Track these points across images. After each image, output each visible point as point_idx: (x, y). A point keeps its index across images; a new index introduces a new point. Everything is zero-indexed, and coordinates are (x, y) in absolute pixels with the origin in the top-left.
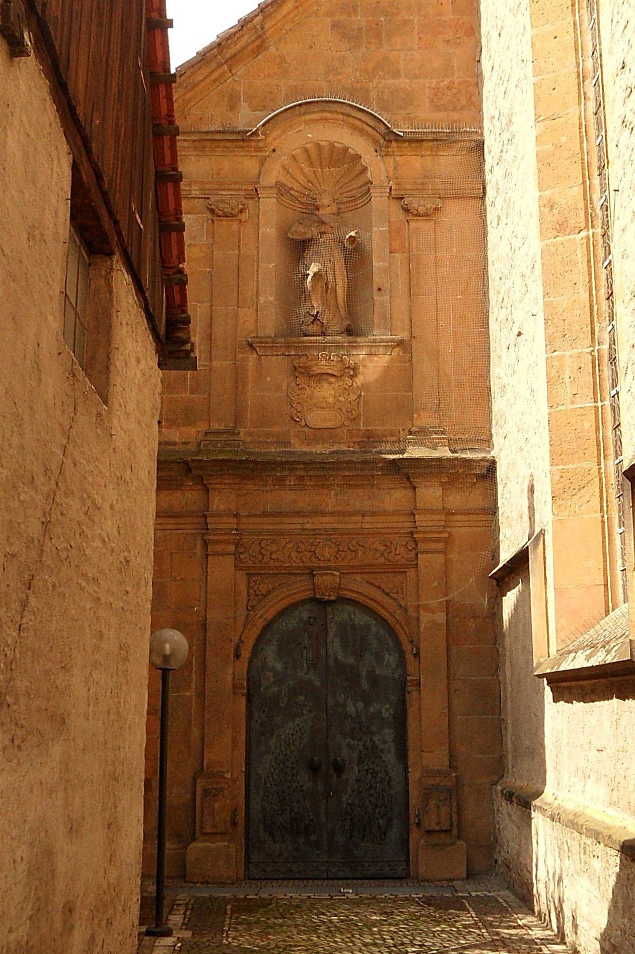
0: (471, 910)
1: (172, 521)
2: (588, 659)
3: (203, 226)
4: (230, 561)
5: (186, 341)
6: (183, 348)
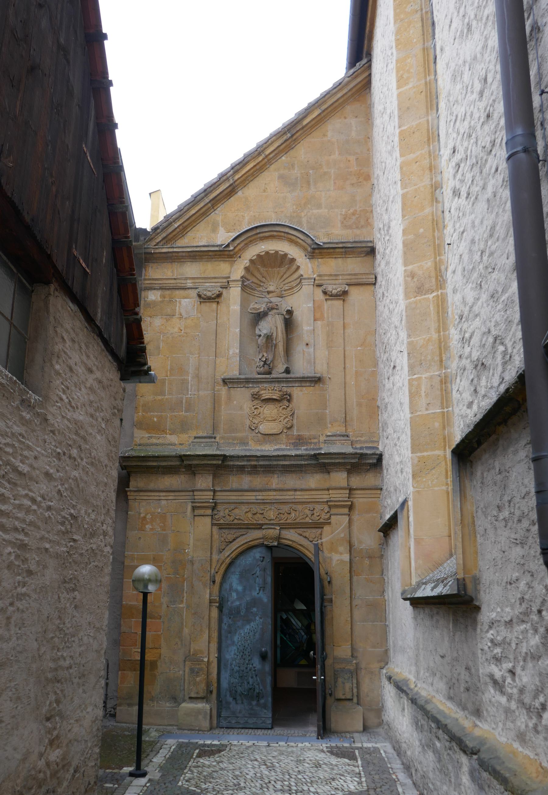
0: (359, 760)
1: (172, 494)
2: (432, 589)
3: (194, 305)
4: (208, 520)
5: (146, 364)
6: (142, 368)
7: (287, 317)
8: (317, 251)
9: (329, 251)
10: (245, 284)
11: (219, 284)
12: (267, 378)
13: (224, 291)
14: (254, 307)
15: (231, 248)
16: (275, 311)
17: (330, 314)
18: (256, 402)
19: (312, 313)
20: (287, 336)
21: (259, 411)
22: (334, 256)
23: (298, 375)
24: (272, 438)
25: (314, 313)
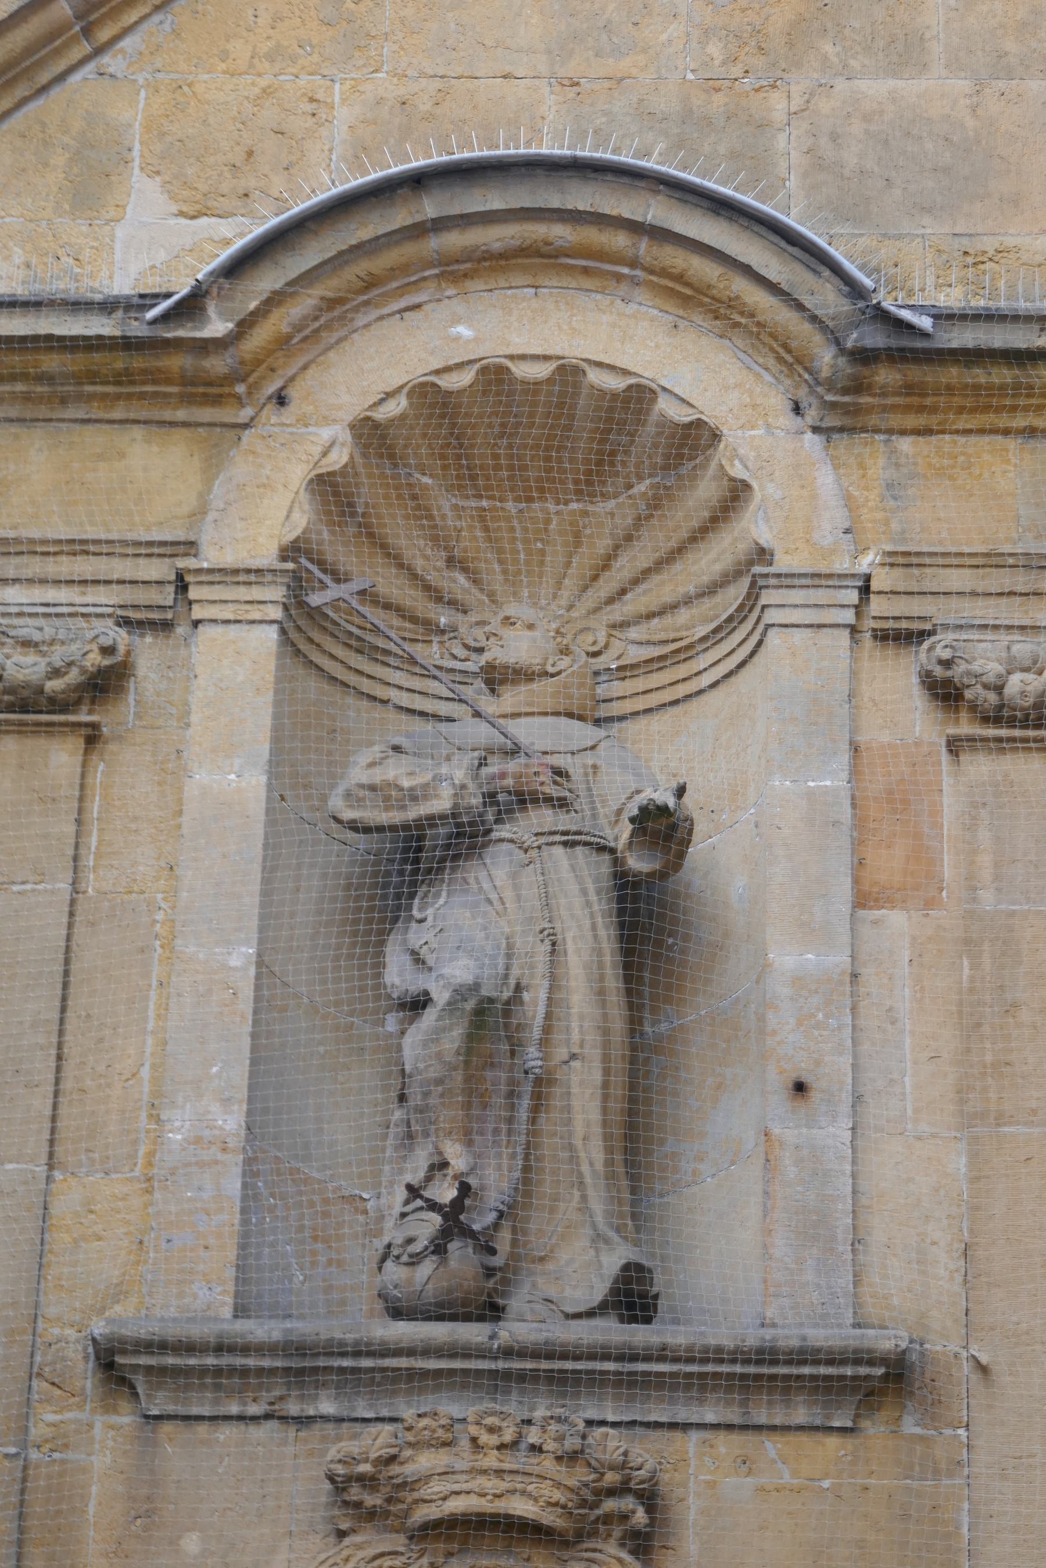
7: (638, 863)
8: (890, 372)
9: (979, 375)
10: (315, 599)
11: (104, 597)
12: (466, 1352)
13: (148, 656)
14: (377, 776)
15: (217, 326)
16: (544, 818)
17: (985, 860)
19: (844, 841)
20: (634, 1023)
22: (1020, 421)
23: (722, 1337)
25: (858, 844)
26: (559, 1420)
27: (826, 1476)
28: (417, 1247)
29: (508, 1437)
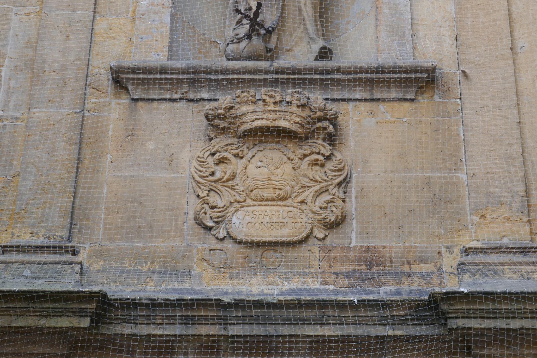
12: (261, 72)
18: (221, 142)
21: (229, 169)
24: (271, 254)
26: (298, 93)
27: (405, 117)
28: (241, 36)
29: (278, 99)
